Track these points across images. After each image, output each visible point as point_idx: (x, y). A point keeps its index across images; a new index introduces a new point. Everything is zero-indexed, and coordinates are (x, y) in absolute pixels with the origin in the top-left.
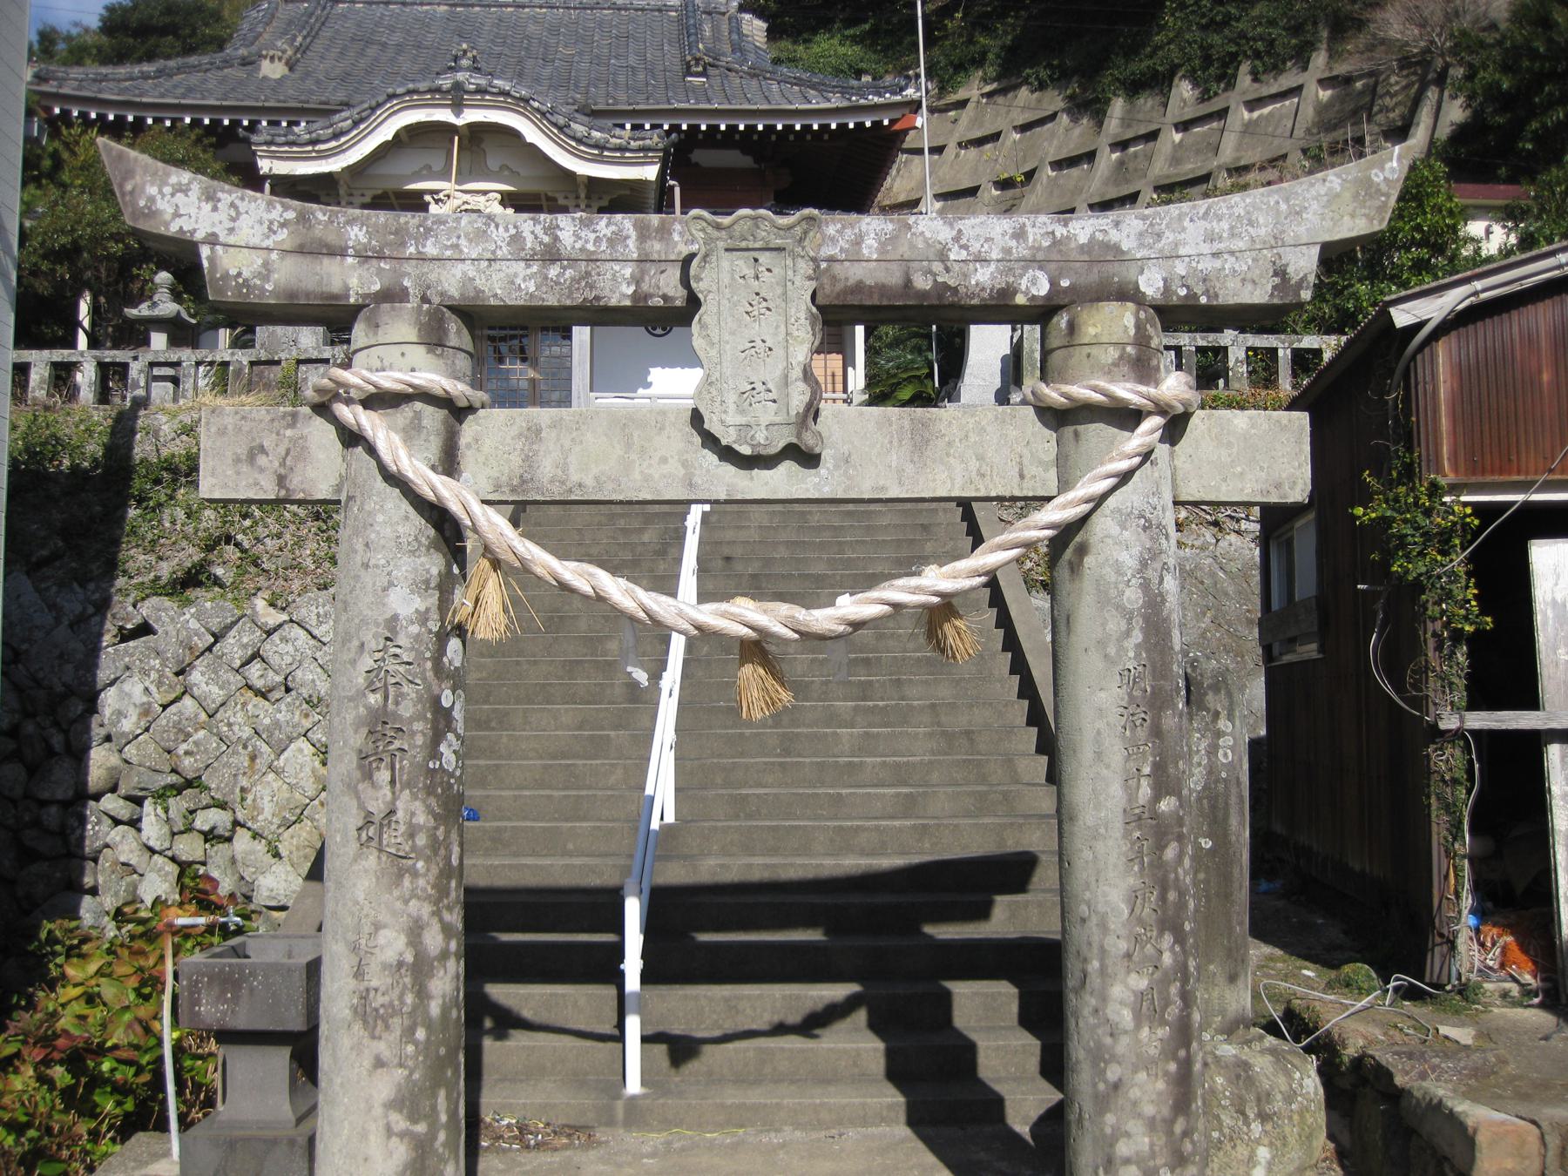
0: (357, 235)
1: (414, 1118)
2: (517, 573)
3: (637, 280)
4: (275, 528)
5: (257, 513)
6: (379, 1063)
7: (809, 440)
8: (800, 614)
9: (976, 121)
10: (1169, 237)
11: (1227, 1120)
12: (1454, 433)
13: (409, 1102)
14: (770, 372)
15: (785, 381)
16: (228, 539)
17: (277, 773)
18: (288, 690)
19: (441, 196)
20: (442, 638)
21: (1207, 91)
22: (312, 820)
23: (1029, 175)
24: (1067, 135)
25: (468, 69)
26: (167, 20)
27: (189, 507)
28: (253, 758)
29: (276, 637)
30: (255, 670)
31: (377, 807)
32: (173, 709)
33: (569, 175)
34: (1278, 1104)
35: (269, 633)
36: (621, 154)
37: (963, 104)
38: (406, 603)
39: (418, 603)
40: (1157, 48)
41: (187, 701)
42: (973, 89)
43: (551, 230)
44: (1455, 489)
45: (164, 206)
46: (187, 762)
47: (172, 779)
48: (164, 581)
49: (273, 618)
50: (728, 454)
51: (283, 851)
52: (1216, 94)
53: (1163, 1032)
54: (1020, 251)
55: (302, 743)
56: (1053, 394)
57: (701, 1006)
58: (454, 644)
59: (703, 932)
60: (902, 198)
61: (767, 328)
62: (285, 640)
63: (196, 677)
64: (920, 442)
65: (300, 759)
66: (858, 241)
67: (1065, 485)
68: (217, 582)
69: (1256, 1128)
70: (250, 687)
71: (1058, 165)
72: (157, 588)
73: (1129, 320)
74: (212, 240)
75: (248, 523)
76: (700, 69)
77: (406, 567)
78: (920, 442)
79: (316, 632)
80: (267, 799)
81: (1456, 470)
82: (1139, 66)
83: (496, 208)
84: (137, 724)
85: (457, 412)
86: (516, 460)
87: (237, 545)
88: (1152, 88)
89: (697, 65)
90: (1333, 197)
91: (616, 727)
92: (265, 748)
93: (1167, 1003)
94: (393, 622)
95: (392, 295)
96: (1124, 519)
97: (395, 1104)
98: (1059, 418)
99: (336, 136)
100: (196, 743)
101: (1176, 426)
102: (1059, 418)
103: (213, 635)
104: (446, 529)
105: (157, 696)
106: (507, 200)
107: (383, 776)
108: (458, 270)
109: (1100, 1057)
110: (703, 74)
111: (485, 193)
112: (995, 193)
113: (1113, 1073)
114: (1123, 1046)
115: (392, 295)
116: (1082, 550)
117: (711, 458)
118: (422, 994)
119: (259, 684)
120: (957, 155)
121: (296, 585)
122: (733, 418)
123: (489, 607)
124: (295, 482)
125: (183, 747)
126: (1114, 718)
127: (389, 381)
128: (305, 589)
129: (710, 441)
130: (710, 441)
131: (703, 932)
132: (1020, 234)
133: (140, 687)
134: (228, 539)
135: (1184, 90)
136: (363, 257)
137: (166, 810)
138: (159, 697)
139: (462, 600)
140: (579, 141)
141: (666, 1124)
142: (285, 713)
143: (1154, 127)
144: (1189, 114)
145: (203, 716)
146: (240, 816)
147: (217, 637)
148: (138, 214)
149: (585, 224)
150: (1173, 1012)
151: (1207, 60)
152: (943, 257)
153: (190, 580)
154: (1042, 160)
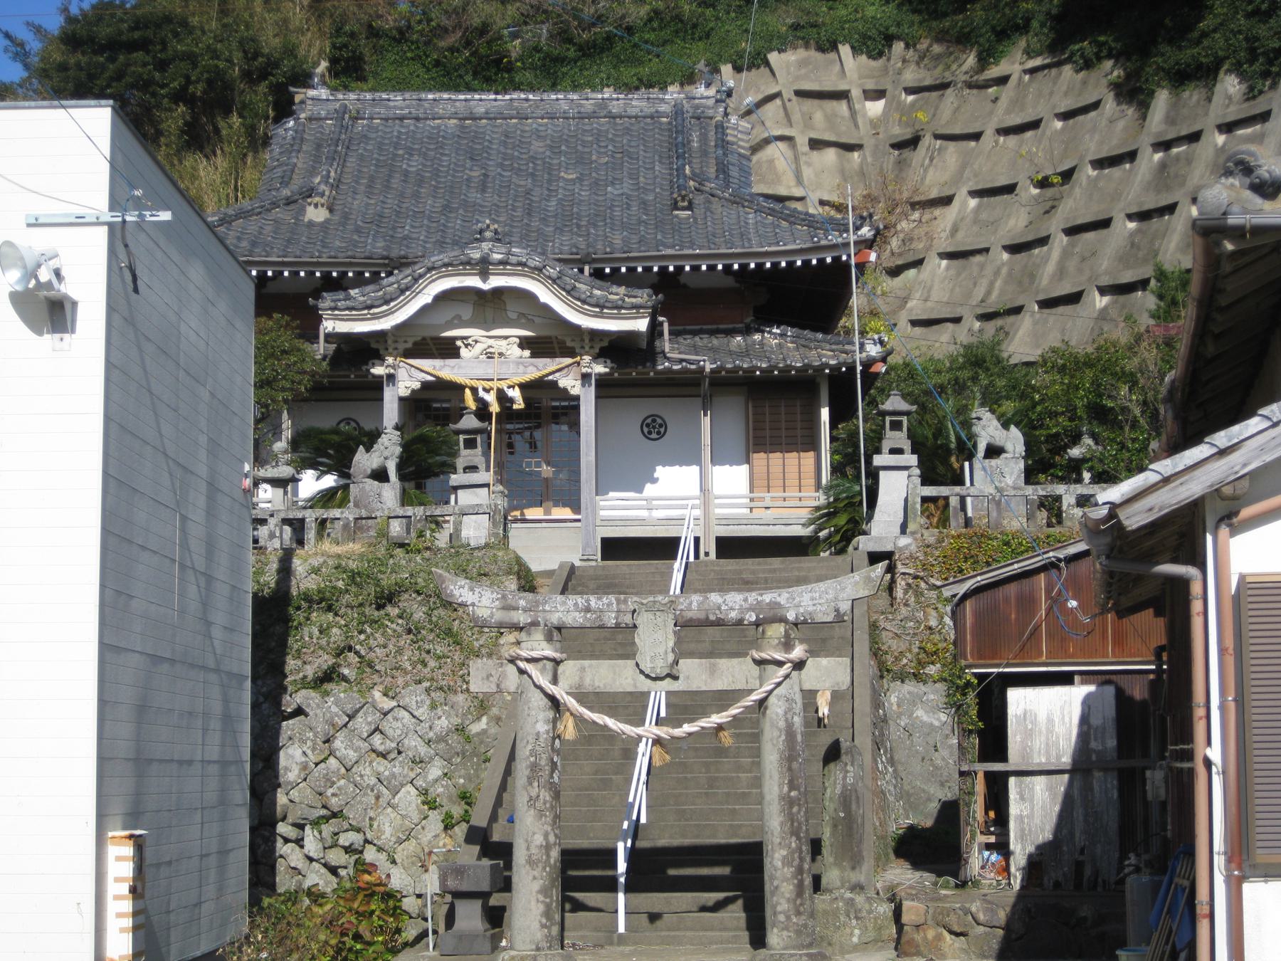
0: (522, 603)
1: (546, 897)
2: (579, 720)
3: (616, 618)
4: (381, 640)
5: (369, 630)
6: (535, 878)
7: (674, 672)
8: (671, 731)
9: (1018, 103)
10: (798, 599)
11: (842, 919)
12: (973, 641)
13: (544, 891)
14: (661, 650)
15: (666, 652)
16: (350, 649)
17: (393, 808)
18: (399, 753)
19: (470, 341)
20: (554, 739)
21: (1251, 89)
22: (417, 839)
23: (1067, 175)
24: (1111, 124)
25: (490, 240)
26: (137, 35)
27: (321, 626)
28: (377, 798)
29: (389, 717)
30: (377, 739)
31: (534, 794)
32: (322, 765)
33: (577, 328)
34: (864, 914)
35: (385, 714)
36: (618, 309)
37: (1003, 80)
38: (542, 727)
39: (546, 727)
40: (1204, 35)
41: (332, 760)
42: (1012, 64)
43: (588, 601)
44: (970, 667)
45: (456, 593)
46: (334, 800)
47: (324, 812)
48: (310, 678)
49: (387, 704)
50: (647, 676)
51: (398, 861)
52: (1261, 92)
53: (792, 869)
54: (745, 605)
55: (409, 788)
56: (756, 655)
57: (655, 901)
58: (557, 741)
59: (652, 869)
60: (934, 194)
61: (659, 636)
62: (396, 719)
63: (338, 744)
64: (713, 671)
65: (409, 798)
66: (691, 604)
67: (761, 686)
68: (345, 679)
69: (854, 922)
70: (374, 751)
71: (1100, 164)
72: (304, 684)
73: (782, 630)
74: (473, 604)
75: (362, 637)
76: (686, 204)
77: (541, 716)
78: (713, 671)
79: (416, 713)
80: (387, 826)
81: (972, 656)
82: (1187, 55)
83: (515, 351)
84: (299, 776)
85: (557, 662)
86: (577, 678)
87: (357, 653)
88: (1199, 79)
89: (683, 200)
90: (856, 583)
91: (616, 774)
92: (385, 791)
93: (793, 860)
94: (538, 734)
95: (535, 624)
96: (779, 697)
97: (540, 892)
98: (760, 663)
99: (387, 302)
100: (339, 788)
101: (799, 665)
102: (760, 663)
103: (348, 716)
104: (555, 702)
105: (312, 757)
106: (524, 343)
107: (536, 784)
108: (557, 615)
109: (772, 878)
110: (690, 207)
111: (506, 338)
112: (1035, 191)
113: (776, 883)
114: (778, 874)
115: (535, 624)
116: (766, 708)
117: (643, 677)
118: (548, 856)
119: (381, 748)
120: (997, 142)
121: (400, 681)
122: (649, 665)
123: (569, 729)
124: (503, 686)
125: (330, 792)
126: (776, 764)
127: (535, 654)
128: (406, 685)
129: (642, 672)
130: (642, 672)
131: (652, 869)
132: (746, 600)
133: (300, 751)
134: (350, 649)
135: (1230, 85)
136: (525, 610)
137: (320, 833)
138: (313, 758)
139: (560, 727)
140: (584, 302)
141: (636, 943)
142: (398, 768)
143: (1196, 128)
144: (1233, 114)
145: (343, 771)
146: (369, 837)
147: (351, 717)
148: (447, 595)
149: (599, 599)
150: (796, 863)
151: (1253, 55)
152: (719, 608)
153: (328, 677)
154: (1082, 158)
